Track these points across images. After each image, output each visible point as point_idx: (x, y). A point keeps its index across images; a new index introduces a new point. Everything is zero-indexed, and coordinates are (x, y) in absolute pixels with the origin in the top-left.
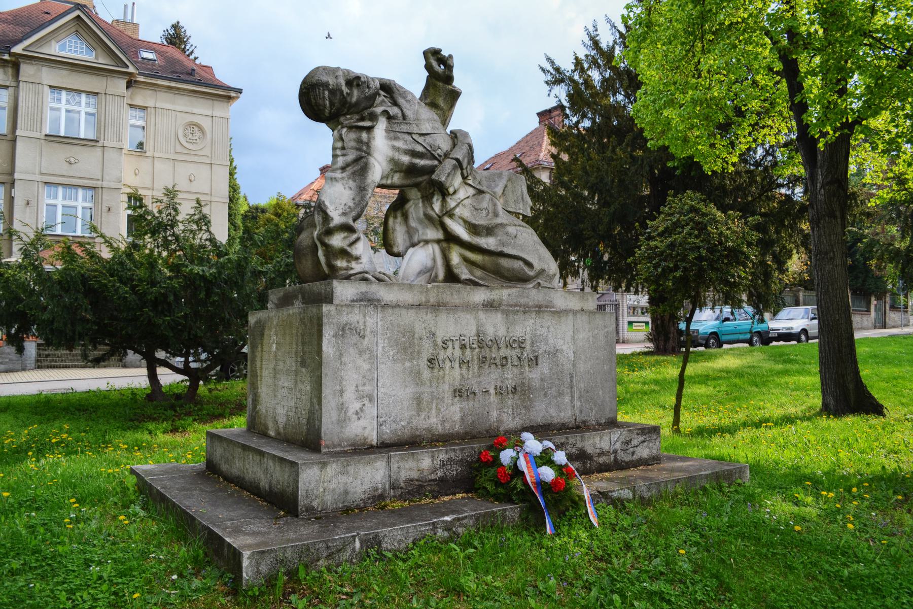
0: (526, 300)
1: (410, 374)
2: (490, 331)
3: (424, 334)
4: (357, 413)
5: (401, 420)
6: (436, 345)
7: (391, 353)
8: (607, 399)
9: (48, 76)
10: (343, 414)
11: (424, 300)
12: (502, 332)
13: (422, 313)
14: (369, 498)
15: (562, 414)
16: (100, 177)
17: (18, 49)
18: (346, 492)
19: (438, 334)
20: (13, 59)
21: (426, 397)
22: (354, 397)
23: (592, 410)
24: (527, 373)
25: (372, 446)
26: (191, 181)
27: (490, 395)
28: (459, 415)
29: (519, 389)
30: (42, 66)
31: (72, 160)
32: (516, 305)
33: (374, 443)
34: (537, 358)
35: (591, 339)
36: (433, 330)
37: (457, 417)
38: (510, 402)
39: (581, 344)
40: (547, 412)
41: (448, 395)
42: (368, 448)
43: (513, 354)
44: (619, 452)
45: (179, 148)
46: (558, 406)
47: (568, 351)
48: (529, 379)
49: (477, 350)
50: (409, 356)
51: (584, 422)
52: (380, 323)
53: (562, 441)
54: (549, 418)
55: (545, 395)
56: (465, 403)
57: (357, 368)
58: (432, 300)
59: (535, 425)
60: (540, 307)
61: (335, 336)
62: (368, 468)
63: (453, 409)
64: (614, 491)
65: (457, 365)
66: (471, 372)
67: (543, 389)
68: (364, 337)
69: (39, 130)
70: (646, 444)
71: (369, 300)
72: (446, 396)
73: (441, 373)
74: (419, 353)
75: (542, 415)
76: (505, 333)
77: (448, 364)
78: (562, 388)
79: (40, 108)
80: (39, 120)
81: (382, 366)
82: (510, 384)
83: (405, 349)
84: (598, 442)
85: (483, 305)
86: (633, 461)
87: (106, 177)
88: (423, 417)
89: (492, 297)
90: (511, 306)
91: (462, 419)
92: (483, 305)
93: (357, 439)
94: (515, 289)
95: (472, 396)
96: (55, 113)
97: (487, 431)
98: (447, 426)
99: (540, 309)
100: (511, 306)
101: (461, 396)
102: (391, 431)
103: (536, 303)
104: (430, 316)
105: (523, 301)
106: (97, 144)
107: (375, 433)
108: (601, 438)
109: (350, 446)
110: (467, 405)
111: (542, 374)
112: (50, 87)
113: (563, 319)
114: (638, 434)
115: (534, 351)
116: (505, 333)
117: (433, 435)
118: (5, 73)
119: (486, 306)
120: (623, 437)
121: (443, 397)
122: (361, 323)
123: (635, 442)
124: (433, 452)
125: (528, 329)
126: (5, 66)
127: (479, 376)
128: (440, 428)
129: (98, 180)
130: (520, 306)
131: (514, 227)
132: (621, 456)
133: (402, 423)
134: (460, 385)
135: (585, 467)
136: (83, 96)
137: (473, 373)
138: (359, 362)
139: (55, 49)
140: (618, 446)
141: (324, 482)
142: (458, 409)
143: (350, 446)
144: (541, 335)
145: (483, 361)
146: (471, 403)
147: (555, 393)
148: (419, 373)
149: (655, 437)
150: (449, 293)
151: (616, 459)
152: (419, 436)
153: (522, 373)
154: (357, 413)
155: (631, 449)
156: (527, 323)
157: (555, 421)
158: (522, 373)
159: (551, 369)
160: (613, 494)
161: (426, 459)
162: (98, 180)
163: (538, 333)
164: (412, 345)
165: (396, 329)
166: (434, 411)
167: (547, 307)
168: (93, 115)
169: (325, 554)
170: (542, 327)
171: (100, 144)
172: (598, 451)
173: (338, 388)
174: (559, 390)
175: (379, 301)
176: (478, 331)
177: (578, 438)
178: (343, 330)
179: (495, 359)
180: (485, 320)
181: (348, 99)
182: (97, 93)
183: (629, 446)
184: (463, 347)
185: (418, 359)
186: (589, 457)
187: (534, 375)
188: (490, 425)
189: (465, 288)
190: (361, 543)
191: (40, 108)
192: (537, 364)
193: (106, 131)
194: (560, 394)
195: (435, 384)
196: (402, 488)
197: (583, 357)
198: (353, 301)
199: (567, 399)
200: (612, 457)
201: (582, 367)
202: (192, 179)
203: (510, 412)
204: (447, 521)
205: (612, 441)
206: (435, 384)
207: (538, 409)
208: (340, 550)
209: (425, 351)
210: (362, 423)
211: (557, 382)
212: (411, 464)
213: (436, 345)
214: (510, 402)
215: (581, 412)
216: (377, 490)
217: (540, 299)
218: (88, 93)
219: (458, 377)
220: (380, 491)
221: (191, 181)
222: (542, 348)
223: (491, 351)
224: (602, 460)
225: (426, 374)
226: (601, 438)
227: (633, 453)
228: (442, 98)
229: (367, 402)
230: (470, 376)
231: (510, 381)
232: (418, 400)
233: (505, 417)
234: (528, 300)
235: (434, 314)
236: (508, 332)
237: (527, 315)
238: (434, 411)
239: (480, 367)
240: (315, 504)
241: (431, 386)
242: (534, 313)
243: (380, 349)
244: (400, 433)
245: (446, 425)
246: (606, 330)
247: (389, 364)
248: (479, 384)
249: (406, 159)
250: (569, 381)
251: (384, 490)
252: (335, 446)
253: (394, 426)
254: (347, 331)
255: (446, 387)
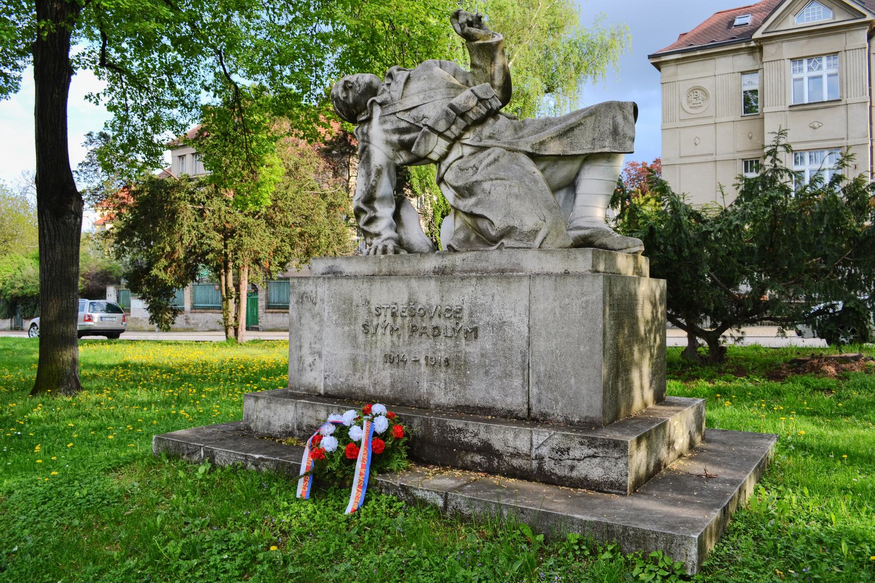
0: (484, 264)
1: (348, 337)
2: (422, 300)
3: (361, 302)
4: (310, 366)
5: (340, 377)
6: (370, 312)
7: (334, 318)
8: (584, 392)
9: (789, 49)
10: (301, 365)
11: (377, 270)
12: (435, 300)
13: (359, 283)
14: (283, 432)
15: (509, 400)
16: (845, 136)
17: (758, 35)
18: (269, 423)
19: (372, 302)
20: (758, 44)
21: (361, 360)
22: (309, 352)
23: (557, 402)
24: (464, 346)
25: (320, 395)
26: (696, 144)
27: (421, 365)
28: (389, 380)
29: (452, 362)
30: (782, 42)
31: (816, 125)
32: (472, 271)
33: (322, 392)
34: (475, 330)
35: (557, 311)
36: (368, 299)
37: (388, 382)
38: (442, 375)
39: (541, 316)
40: (488, 393)
41: (380, 360)
42: (318, 396)
43: (446, 324)
44: (547, 459)
45: (683, 116)
46: (504, 389)
47: (519, 324)
48: (466, 353)
49: (408, 318)
50: (348, 321)
51: (544, 415)
52: (327, 292)
53: (461, 426)
54: (490, 401)
55: (487, 373)
56: (395, 370)
57: (311, 329)
58: (384, 270)
59: (472, 405)
60: (503, 271)
61: (297, 302)
62: (283, 408)
63: (384, 373)
64: (416, 489)
65: (388, 331)
66: (401, 340)
67: (485, 366)
68: (315, 304)
69: (783, 104)
70: (597, 460)
71: (334, 273)
72: (378, 360)
73: (373, 339)
74: (356, 319)
75: (481, 395)
76: (439, 302)
77: (380, 331)
78: (510, 368)
79: (783, 82)
80: (783, 94)
81: (328, 329)
82: (442, 356)
83: (344, 315)
84: (511, 439)
85: (434, 272)
86: (571, 478)
87: (851, 135)
88: (357, 376)
89: (444, 263)
90: (466, 272)
91: (392, 385)
92: (434, 272)
93: (311, 386)
94: (472, 253)
95: (401, 364)
96: (799, 82)
97: (416, 401)
98: (378, 389)
99: (503, 274)
100: (466, 272)
101: (391, 363)
102: (333, 385)
103: (498, 267)
104: (366, 285)
105: (480, 265)
106: (840, 103)
107: (322, 384)
108: (516, 436)
109: (306, 391)
110: (398, 372)
111: (482, 348)
112: (791, 59)
113: (514, 286)
114: (582, 444)
115: (473, 322)
116: (439, 302)
117: (365, 395)
118: (754, 58)
119: (437, 273)
120: (555, 442)
121: (375, 361)
122: (314, 292)
123: (576, 453)
124: (328, 406)
125: (466, 297)
126: (753, 52)
127: (410, 344)
128: (372, 389)
129: (843, 139)
130: (477, 271)
131: (490, 182)
132: (548, 465)
133: (341, 379)
134: (391, 351)
135: (491, 465)
136: (824, 59)
137: (404, 341)
138: (312, 324)
139: (793, 23)
140: (545, 451)
141: (257, 411)
142: (389, 375)
143: (306, 391)
144: (482, 304)
145: (413, 329)
146: (401, 371)
147: (499, 373)
148: (355, 337)
149: (616, 455)
150: (399, 262)
151: (540, 468)
152: (354, 393)
153: (457, 346)
154: (310, 366)
155: (569, 462)
156: (465, 291)
157: (499, 406)
158: (457, 346)
159: (495, 344)
160: (416, 492)
161: (323, 411)
162: (843, 139)
163: (479, 302)
164: (350, 311)
165: (338, 297)
166: (367, 373)
167: (512, 271)
168: (836, 75)
169: (186, 452)
170: (484, 295)
171: (843, 102)
172: (511, 450)
173: (298, 344)
174: (505, 370)
175: (341, 273)
176: (410, 301)
177: (482, 428)
178: (302, 298)
179: (425, 328)
180: (417, 288)
181: (347, 102)
182: (837, 53)
183: (566, 457)
184: (394, 315)
185: (355, 324)
186: (499, 455)
187: (472, 349)
188: (420, 396)
189: (416, 256)
190: (204, 452)
191: (783, 82)
192: (476, 338)
193: (849, 88)
194: (507, 375)
195: (368, 349)
196: (304, 431)
197: (544, 333)
198: (323, 274)
199: (517, 382)
200: (535, 464)
201: (541, 345)
202: (697, 141)
203: (442, 385)
204: (254, 458)
205: (535, 443)
206: (368, 349)
207: (477, 388)
208: (193, 453)
209: (361, 317)
210: (314, 374)
211: (503, 360)
212: (310, 412)
213: (370, 312)
214: (442, 375)
215: (539, 401)
216: (288, 427)
217: (504, 261)
218: (828, 55)
219: (389, 344)
220: (290, 429)
221: (696, 144)
222: (483, 319)
223: (423, 320)
224: (516, 462)
225: (361, 338)
226: (516, 436)
227: (572, 468)
228: (476, 56)
229: (317, 358)
230: (400, 344)
231: (443, 353)
232: (354, 361)
233: (436, 390)
234: (488, 264)
235: (369, 284)
236: (442, 301)
237: (465, 282)
238: (367, 373)
239: (410, 336)
240: (252, 426)
241: (365, 350)
242: (475, 280)
243: (326, 314)
244: (339, 388)
245: (377, 388)
246: (585, 299)
247: (332, 327)
248: (410, 352)
249: (395, 138)
250: (520, 360)
251: (293, 428)
252: (296, 389)
253: (335, 381)
254: (305, 299)
255: (378, 352)
